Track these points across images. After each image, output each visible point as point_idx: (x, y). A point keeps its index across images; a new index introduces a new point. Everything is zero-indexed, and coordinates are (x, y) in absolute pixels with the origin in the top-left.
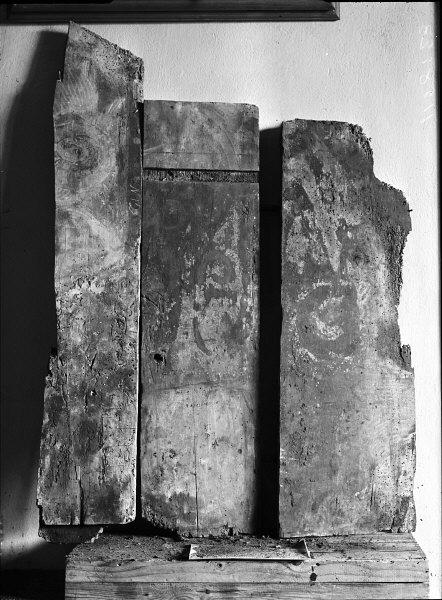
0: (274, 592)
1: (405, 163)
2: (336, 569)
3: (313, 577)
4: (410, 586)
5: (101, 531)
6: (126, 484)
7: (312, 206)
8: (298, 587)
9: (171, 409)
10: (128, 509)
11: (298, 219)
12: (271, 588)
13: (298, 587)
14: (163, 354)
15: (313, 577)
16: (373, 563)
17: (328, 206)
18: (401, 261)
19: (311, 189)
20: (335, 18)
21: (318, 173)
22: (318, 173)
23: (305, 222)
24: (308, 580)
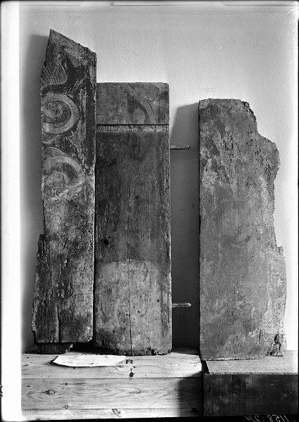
0: (108, 384)
1: (278, 125)
2: (145, 370)
3: (132, 375)
4: (83, 369)
5: (71, 346)
6: (86, 321)
7: (219, 152)
8: (122, 381)
9: (116, 272)
10: (88, 332)
11: (210, 161)
12: (105, 381)
13: (122, 381)
14: (110, 240)
15: (132, 375)
16: (168, 366)
17: (229, 152)
18: (275, 177)
19: (219, 142)
20: (52, 32)
21: (223, 132)
22: (223, 132)
23: (214, 162)
24: (128, 377)
